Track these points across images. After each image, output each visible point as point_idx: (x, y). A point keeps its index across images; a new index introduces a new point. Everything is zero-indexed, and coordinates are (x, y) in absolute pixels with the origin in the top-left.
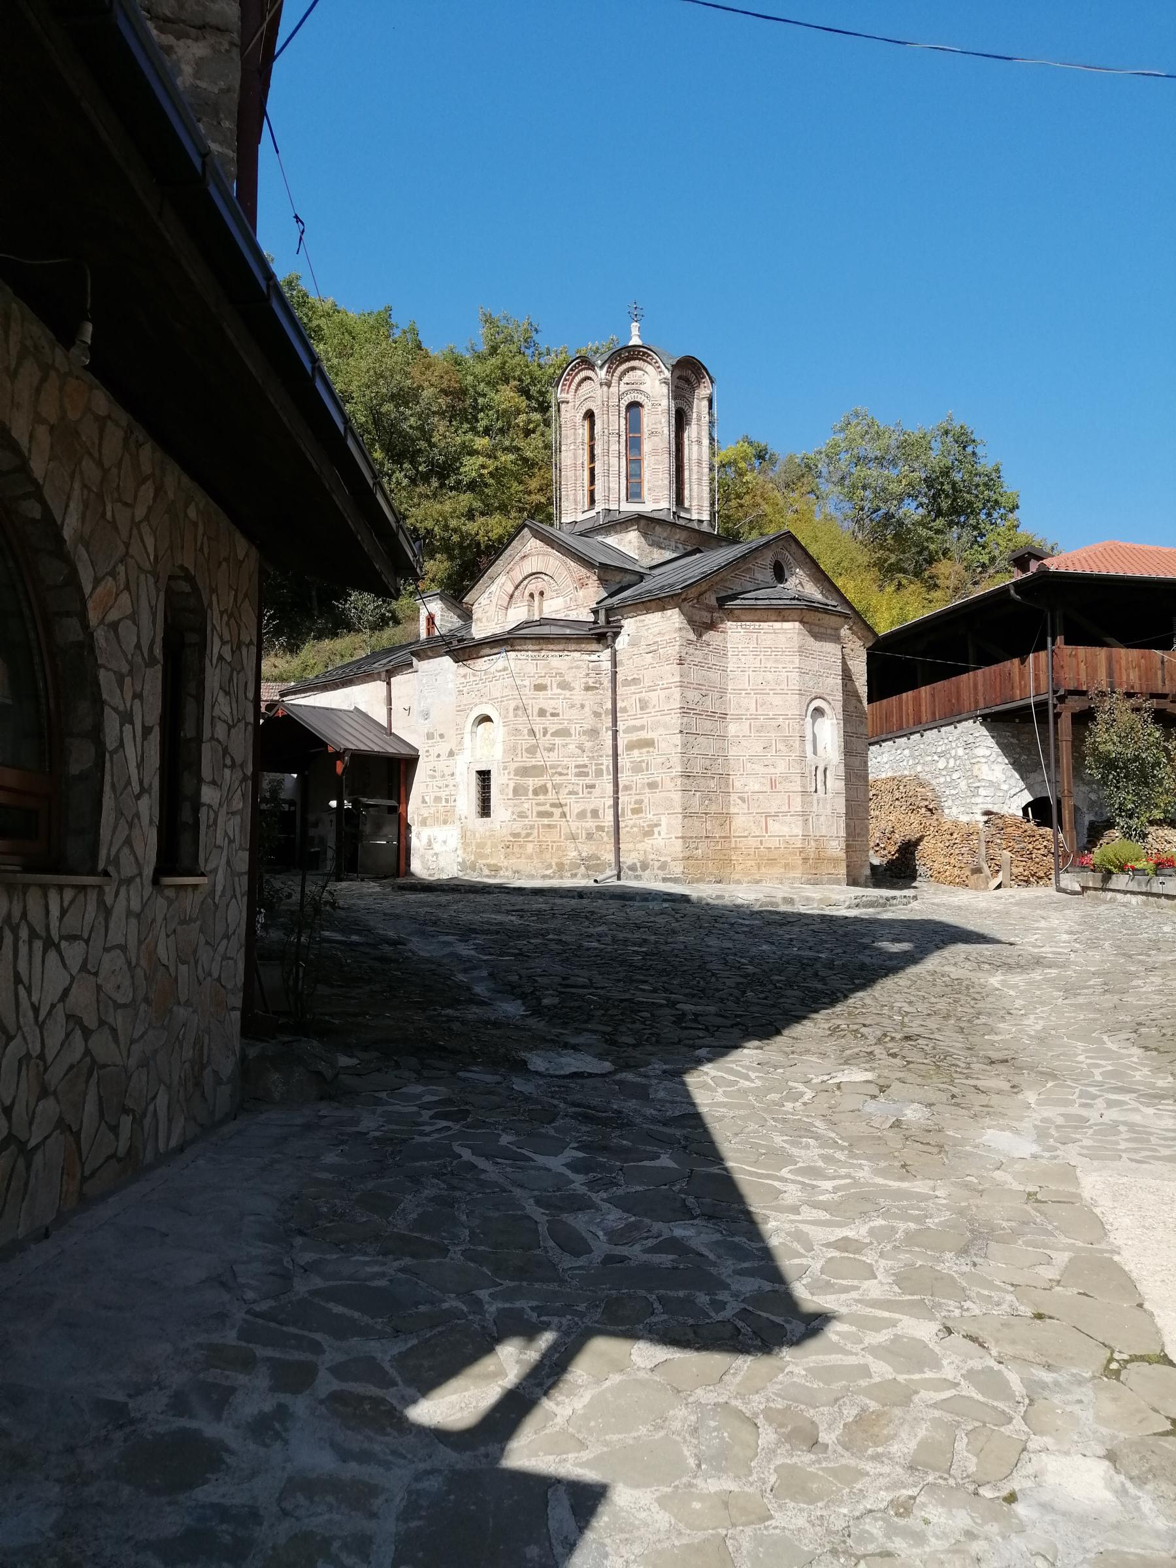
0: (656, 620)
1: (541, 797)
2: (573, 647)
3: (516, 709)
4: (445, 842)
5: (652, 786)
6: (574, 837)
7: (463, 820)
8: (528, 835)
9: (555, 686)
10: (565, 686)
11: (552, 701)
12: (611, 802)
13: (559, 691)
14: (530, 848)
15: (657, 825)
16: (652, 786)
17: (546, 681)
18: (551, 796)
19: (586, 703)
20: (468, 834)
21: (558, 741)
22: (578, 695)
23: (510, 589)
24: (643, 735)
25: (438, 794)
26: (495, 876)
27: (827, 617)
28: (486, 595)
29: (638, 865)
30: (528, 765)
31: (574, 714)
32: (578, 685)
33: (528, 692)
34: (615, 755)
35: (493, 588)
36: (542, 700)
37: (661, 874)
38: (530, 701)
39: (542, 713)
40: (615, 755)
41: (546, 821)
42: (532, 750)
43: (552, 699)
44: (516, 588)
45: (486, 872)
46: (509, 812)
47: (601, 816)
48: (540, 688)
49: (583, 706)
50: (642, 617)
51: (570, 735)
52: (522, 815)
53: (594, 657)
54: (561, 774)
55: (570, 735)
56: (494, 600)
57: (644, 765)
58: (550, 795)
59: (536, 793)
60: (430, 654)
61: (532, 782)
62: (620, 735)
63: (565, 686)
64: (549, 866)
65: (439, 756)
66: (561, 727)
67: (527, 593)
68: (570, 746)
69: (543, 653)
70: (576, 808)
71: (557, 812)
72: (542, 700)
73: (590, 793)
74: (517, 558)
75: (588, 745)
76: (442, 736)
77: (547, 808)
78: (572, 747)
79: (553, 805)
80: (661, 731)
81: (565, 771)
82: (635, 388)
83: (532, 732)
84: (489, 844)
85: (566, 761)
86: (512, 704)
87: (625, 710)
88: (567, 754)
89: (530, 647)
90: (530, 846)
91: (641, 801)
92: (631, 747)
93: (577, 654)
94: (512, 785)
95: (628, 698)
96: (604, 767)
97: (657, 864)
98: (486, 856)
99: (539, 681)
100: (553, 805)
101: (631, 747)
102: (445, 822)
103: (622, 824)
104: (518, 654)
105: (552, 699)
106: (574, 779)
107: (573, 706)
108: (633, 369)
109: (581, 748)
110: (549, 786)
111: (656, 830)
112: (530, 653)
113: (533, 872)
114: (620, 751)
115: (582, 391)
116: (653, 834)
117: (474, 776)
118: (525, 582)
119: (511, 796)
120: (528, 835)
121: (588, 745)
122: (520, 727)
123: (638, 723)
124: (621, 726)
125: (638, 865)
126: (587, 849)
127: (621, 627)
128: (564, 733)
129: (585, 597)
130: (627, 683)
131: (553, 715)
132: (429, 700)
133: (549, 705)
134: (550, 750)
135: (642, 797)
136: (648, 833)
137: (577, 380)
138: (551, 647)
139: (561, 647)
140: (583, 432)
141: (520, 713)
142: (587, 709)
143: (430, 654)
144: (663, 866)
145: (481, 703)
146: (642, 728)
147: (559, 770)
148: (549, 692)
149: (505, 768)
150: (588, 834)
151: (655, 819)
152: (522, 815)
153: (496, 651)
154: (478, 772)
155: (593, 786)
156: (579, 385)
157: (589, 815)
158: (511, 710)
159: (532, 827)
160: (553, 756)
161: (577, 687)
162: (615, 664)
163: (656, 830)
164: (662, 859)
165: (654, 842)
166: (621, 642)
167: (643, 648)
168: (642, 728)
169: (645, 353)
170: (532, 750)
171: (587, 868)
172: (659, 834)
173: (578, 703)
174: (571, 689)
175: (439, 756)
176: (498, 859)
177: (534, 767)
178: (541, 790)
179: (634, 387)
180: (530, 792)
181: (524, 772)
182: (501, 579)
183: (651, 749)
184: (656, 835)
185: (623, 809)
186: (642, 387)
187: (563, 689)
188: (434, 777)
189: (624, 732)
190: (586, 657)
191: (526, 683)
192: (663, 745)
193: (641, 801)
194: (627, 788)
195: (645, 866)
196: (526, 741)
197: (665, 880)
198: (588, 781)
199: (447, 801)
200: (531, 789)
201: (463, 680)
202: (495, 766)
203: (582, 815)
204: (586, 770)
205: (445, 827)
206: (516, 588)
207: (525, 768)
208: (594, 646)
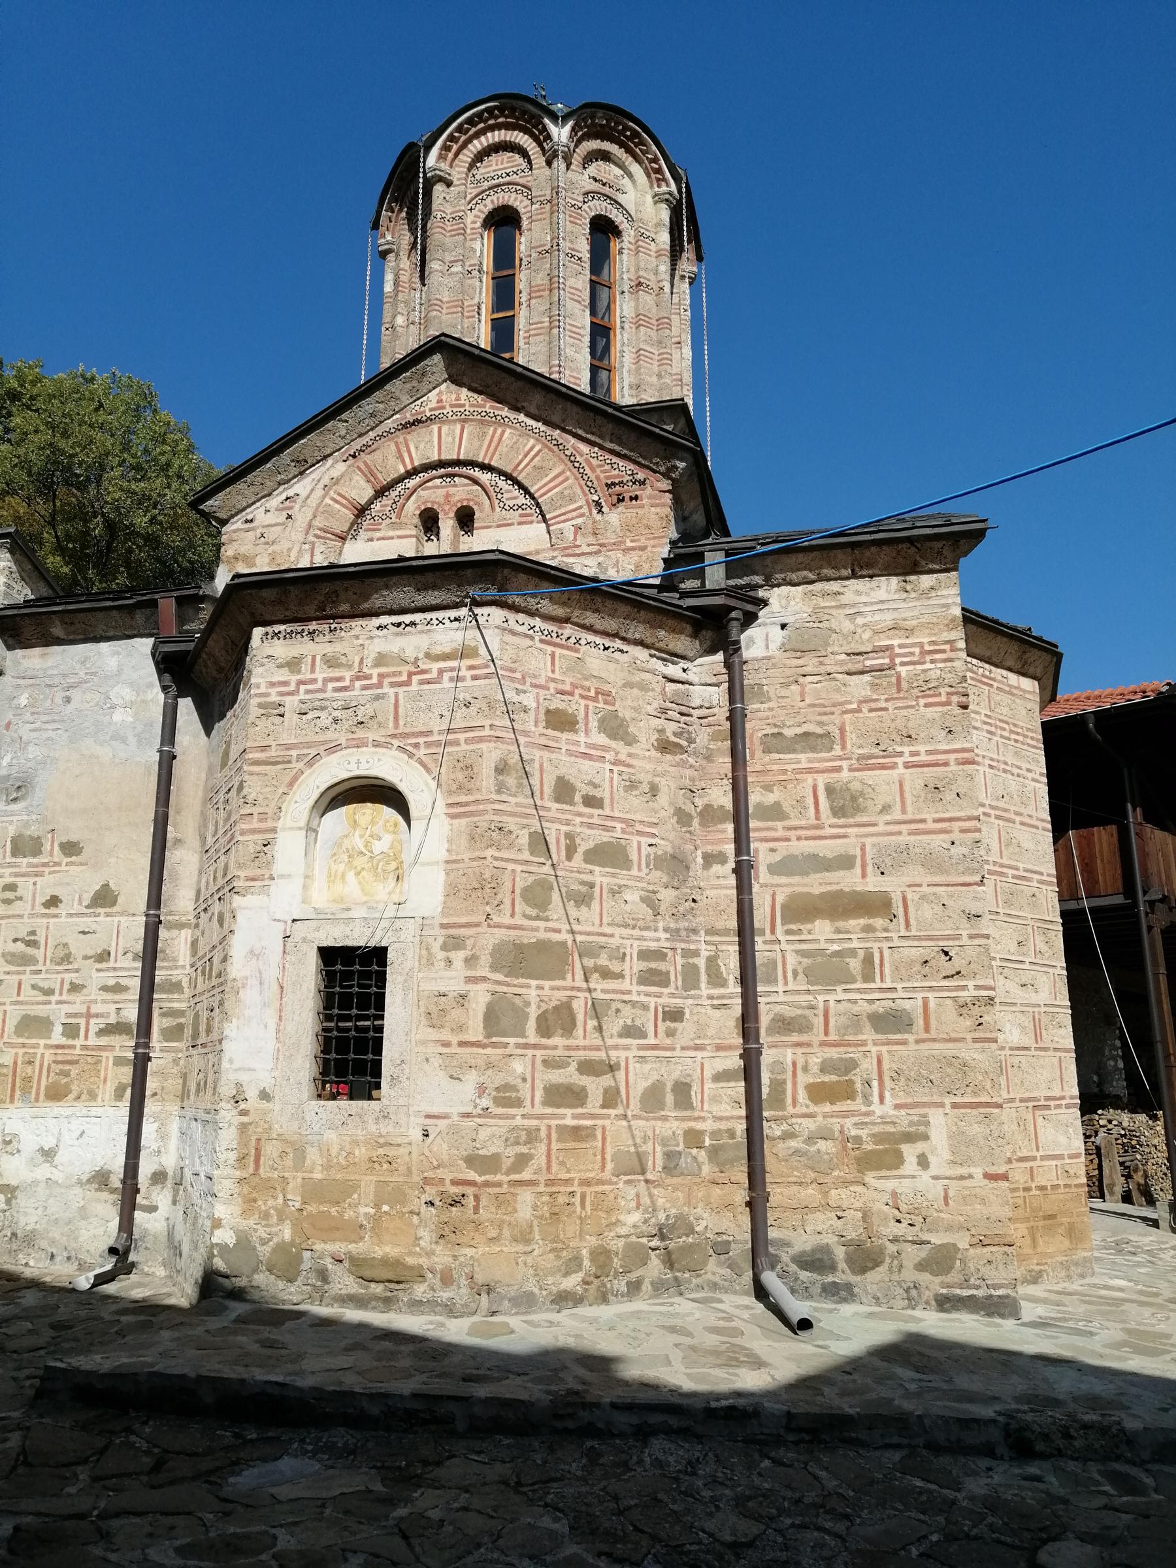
0: (882, 594)
1: (557, 1040)
2: (637, 631)
3: (501, 769)
4: (48, 1154)
5: (891, 1022)
6: (637, 1165)
7: (252, 1101)
8: (522, 1161)
9: (594, 723)
10: (615, 728)
11: (586, 765)
12: (734, 1061)
13: (602, 739)
14: (525, 1204)
15: (910, 1138)
16: (891, 1022)
17: (576, 706)
18: (584, 1035)
19: (662, 782)
20: (271, 1150)
21: (600, 876)
22: (645, 761)
23: (364, 492)
24: (850, 881)
25: (40, 1011)
26: (387, 1303)
27: (587, 762)
28: (274, 502)
29: (840, 1253)
30: (528, 938)
31: (633, 806)
32: (646, 730)
33: (530, 723)
34: (745, 932)
35: (300, 487)
36: (560, 758)
37: (933, 1284)
38: (537, 753)
39: (564, 791)
40: (745, 932)
41: (568, 1117)
42: (537, 897)
43: (580, 758)
44: (380, 493)
45: (345, 1282)
46: (468, 1087)
47: (695, 1100)
48: (560, 721)
49: (654, 790)
50: (834, 586)
51: (626, 863)
52: (507, 1097)
53: (674, 670)
54: (606, 974)
55: (626, 863)
56: (302, 516)
57: (855, 965)
58: (578, 1039)
59: (544, 1029)
60: (57, 631)
61: (536, 994)
62: (762, 878)
63: (615, 728)
64: (574, 1264)
65: (54, 901)
66: (605, 837)
67: (412, 508)
68: (630, 896)
69: (568, 630)
70: (639, 1077)
71: (595, 1086)
72: (560, 758)
73: (670, 1033)
74: (389, 424)
75: (667, 896)
76: (71, 848)
77: (569, 1075)
78: (632, 896)
79: (587, 1068)
80: (914, 873)
81: (615, 967)
82: (605, 192)
83: (540, 843)
84: (368, 1185)
85: (618, 937)
86: (492, 754)
87: (775, 812)
88: (616, 917)
89: (546, 606)
90: (526, 1197)
91: (851, 1065)
92: (801, 911)
93: (641, 654)
94: (480, 997)
95: (776, 779)
96: (701, 963)
97: (913, 1254)
98: (356, 1230)
99: (557, 703)
100: (587, 1068)
101: (801, 911)
102: (56, 1094)
103: (771, 1129)
104: (512, 616)
105: (580, 758)
106: (637, 993)
107: (632, 785)
108: (605, 156)
109: (650, 901)
110: (578, 1006)
111: (910, 1152)
112: (537, 622)
113: (531, 1286)
114: (761, 917)
115: (483, 170)
116: (899, 1160)
117: (311, 963)
118: (411, 483)
119: (475, 1031)
120: (522, 1161)
121: (667, 896)
122: (511, 823)
123: (826, 849)
124: (762, 853)
125: (840, 1253)
126: (668, 1203)
127: (764, 603)
128: (610, 855)
129: (627, 528)
130: (776, 742)
131: (590, 801)
132: (33, 752)
133: (582, 773)
134: (583, 900)
135: (854, 1053)
136: (884, 1154)
137: (477, 145)
138: (591, 618)
139: (611, 625)
140: (483, 247)
141: (511, 781)
142: (663, 799)
143: (57, 631)
144: (940, 1260)
145: (360, 744)
146: (845, 862)
147: (603, 961)
148: (581, 737)
149: (453, 943)
150: (669, 1156)
151: (904, 1121)
152: (507, 1097)
153: (433, 597)
154: (328, 955)
155: (675, 1015)
156: (480, 157)
157: (670, 1098)
158: (486, 770)
159: (532, 1136)
160: (588, 918)
161: (642, 738)
162: (735, 692)
163: (910, 1152)
164: (937, 1239)
165: (904, 1187)
166: (759, 642)
167: (837, 661)
168: (845, 862)
169: (636, 134)
170: (537, 897)
171: (669, 1261)
172: (923, 1162)
173: (645, 778)
174: (630, 741)
175: (54, 901)
176: (418, 1243)
177: (543, 947)
178: (558, 1020)
179: (606, 190)
180: (531, 1025)
181: (520, 959)
182: (334, 468)
183: (879, 922)
184: (910, 1165)
185: (778, 1086)
186: (621, 198)
187: (613, 736)
188: (26, 960)
189: (773, 869)
190: (657, 665)
191: (529, 700)
192: (923, 913)
193: (851, 1065)
194: (784, 1025)
195: (865, 1258)
196: (519, 868)
197: (945, 1303)
198: (667, 998)
199: (71, 1031)
200: (533, 1013)
201: (283, 675)
202: (410, 930)
203: (653, 1099)
204: (661, 966)
205: (57, 1109)
206: (380, 493)
207: (520, 948)
208: (682, 643)
